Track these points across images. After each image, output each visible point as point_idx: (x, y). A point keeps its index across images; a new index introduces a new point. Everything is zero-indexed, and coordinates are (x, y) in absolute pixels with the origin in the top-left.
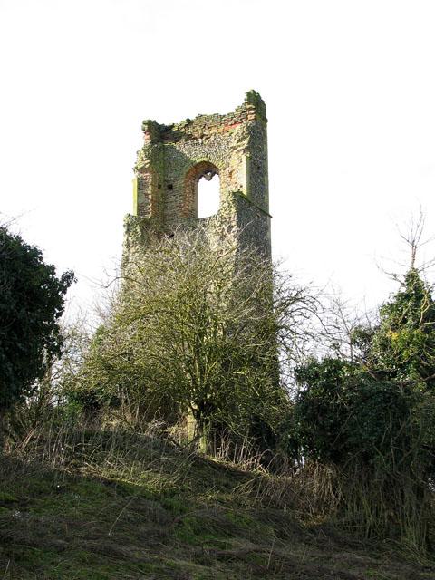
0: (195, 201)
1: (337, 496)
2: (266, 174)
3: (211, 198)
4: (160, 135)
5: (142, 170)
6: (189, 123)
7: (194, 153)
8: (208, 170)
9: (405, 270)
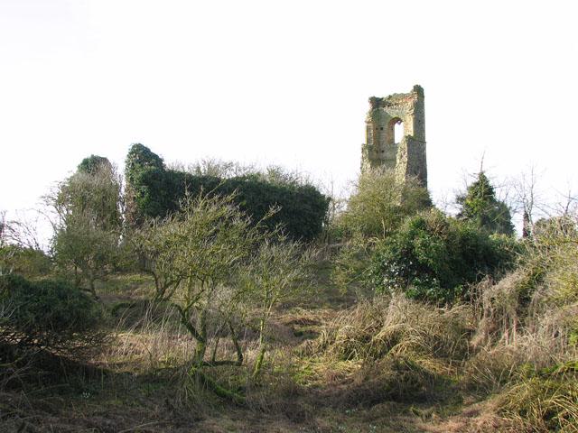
0: (393, 135)
1: (141, 282)
2: (424, 123)
3: (401, 133)
4: (377, 103)
5: (368, 123)
6: (390, 97)
7: (391, 112)
8: (398, 120)
9: (479, 172)
